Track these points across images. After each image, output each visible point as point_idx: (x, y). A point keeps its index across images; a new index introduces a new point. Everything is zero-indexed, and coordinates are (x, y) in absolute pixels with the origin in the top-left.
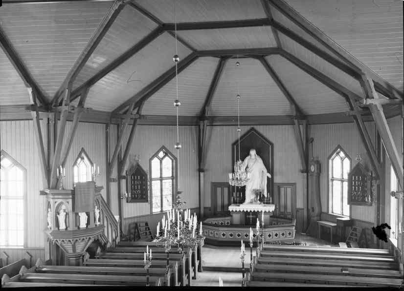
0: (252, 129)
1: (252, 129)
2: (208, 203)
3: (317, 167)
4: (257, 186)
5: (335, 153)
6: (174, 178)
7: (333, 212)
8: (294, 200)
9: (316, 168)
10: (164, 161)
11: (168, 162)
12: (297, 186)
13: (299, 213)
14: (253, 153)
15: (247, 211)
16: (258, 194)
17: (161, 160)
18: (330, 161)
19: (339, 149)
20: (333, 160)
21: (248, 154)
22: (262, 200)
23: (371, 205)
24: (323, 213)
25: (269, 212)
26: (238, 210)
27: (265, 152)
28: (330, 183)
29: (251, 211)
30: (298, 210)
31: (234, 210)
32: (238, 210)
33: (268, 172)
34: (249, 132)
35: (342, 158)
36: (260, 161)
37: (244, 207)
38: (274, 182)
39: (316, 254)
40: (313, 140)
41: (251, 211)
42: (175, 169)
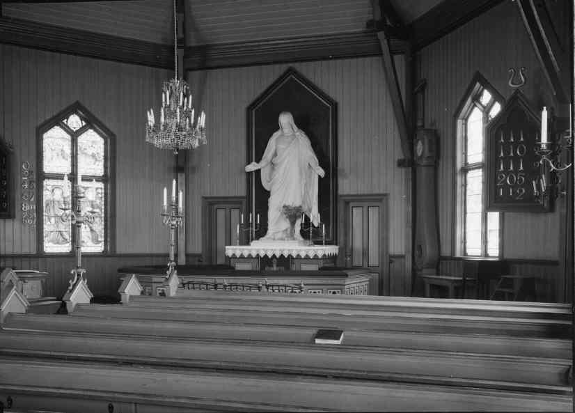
0: (291, 71)
1: (291, 71)
2: (197, 248)
3: (430, 141)
4: (294, 201)
5: (469, 100)
6: (109, 179)
7: (465, 254)
8: (384, 240)
9: (427, 146)
10: (83, 140)
11: (93, 143)
12: (391, 202)
13: (396, 265)
14: (285, 120)
15: (266, 256)
16: (293, 214)
17: (74, 136)
18: (460, 122)
19: (478, 85)
20: (466, 119)
21: (276, 127)
22: (308, 233)
23: (552, 209)
24: (446, 258)
25: (316, 257)
26: (246, 255)
27: (320, 127)
28: (459, 180)
29: (274, 256)
30: (392, 259)
31: (238, 255)
32: (246, 255)
33: (321, 165)
34: (281, 79)
35: (484, 107)
36: (303, 142)
37: (259, 247)
38: (340, 192)
39: (506, 386)
40: (426, 83)
41: (274, 256)
42: (111, 158)
